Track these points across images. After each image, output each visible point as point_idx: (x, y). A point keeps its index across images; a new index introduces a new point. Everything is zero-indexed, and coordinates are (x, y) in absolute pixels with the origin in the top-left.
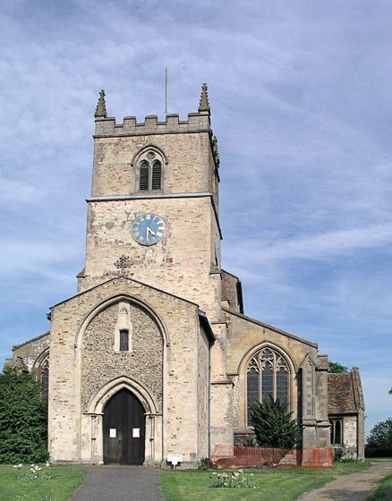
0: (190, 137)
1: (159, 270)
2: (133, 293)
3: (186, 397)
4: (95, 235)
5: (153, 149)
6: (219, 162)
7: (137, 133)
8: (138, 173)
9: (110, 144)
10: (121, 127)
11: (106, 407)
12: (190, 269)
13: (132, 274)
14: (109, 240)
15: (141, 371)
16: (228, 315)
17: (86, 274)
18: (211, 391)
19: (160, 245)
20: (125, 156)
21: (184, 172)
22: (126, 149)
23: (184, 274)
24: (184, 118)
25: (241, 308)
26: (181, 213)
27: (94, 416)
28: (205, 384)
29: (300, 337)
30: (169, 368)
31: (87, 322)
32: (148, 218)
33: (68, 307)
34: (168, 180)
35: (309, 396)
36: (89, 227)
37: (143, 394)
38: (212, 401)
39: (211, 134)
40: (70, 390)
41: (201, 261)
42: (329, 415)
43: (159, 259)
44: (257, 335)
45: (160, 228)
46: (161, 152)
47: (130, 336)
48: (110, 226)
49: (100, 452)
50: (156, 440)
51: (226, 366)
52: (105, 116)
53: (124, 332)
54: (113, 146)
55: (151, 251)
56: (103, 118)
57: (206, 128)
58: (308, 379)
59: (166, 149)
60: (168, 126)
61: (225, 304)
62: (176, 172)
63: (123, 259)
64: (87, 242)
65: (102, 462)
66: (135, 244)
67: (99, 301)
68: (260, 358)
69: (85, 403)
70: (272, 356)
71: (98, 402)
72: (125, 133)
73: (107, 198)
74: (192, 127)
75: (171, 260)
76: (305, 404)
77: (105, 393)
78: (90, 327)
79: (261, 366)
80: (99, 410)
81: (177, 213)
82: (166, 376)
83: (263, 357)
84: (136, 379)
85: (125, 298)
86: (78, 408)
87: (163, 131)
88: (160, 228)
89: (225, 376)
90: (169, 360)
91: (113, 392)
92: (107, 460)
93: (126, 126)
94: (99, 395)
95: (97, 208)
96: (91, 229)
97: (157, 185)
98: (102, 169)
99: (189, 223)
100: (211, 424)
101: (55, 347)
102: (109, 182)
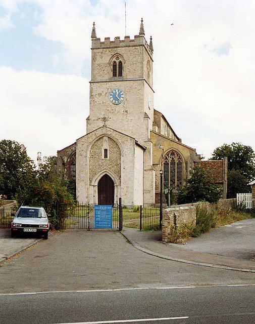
5: (118, 55)
8: (112, 67)
15: (112, 167)
20: (106, 58)
24: (132, 38)
27: (94, 186)
33: (83, 140)
37: (113, 177)
45: (122, 96)
53: (106, 150)
68: (169, 155)
69: (91, 181)
77: (98, 177)
79: (170, 159)
82: (122, 169)
85: (104, 135)
88: (122, 96)
91: (102, 176)
94: (96, 177)
97: (121, 74)
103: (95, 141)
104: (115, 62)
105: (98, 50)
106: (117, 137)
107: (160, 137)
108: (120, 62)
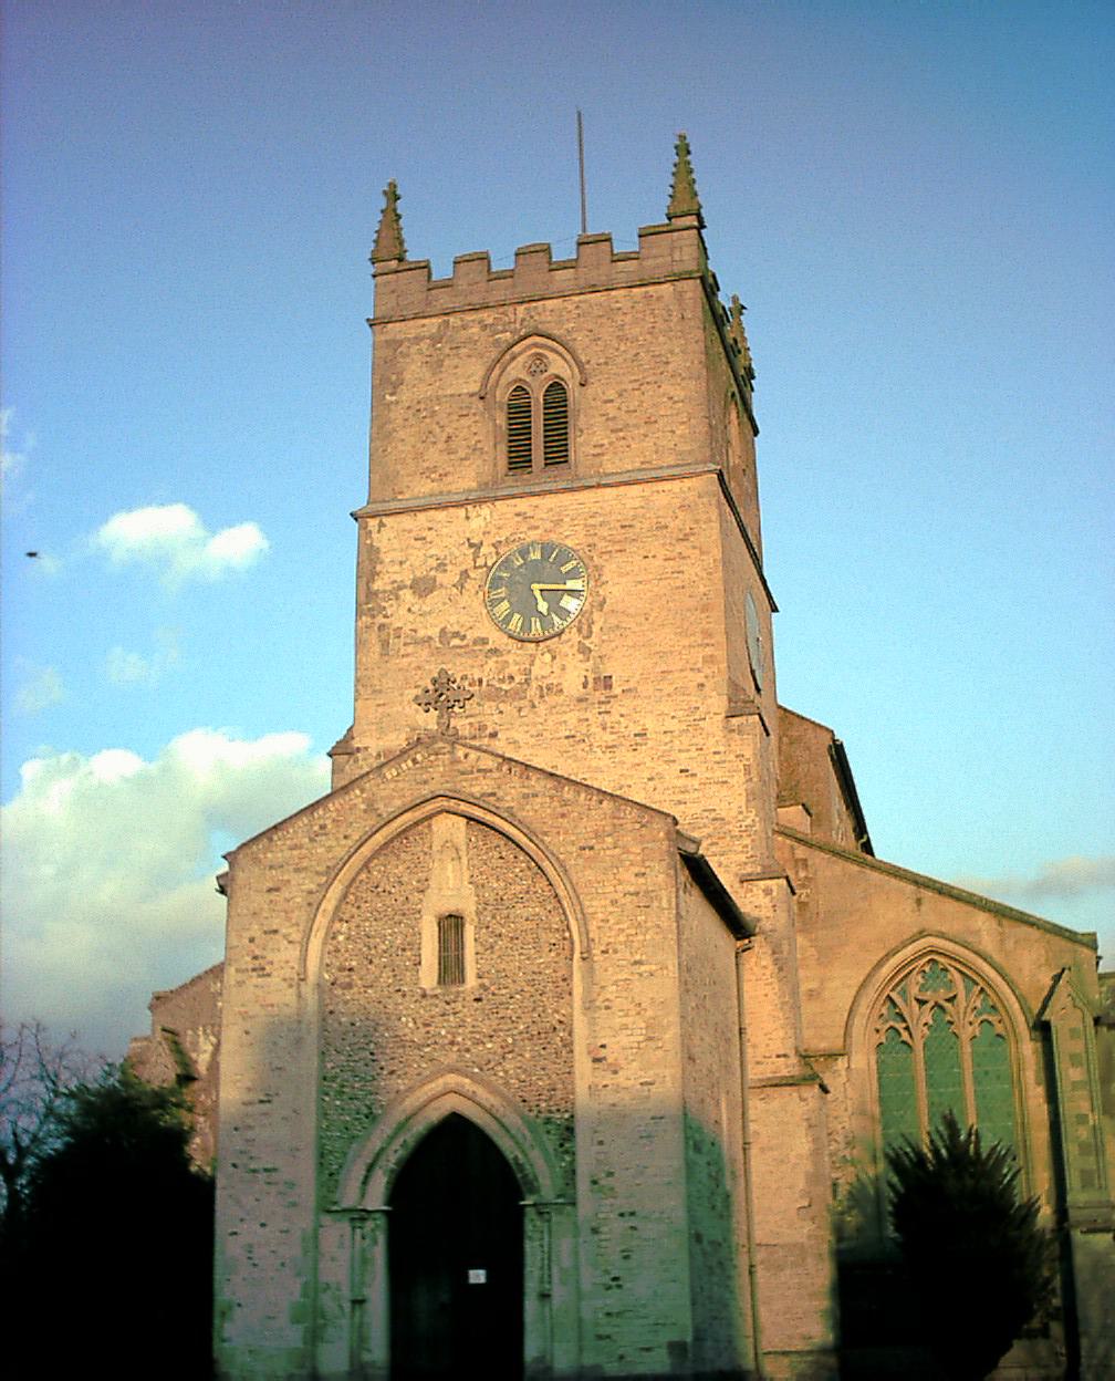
4: (380, 620)
6: (750, 374)
8: (502, 420)
9: (418, 340)
10: (446, 285)
12: (666, 707)
13: (494, 735)
14: (421, 633)
15: (507, 1050)
16: (801, 852)
17: (356, 744)
18: (752, 1114)
19: (573, 636)
21: (634, 405)
22: (463, 351)
23: (650, 723)
25: (860, 828)
26: (630, 534)
27: (360, 1216)
28: (1022, 1192)
30: (593, 1034)
31: (336, 890)
32: (536, 556)
33: (279, 852)
34: (586, 438)
35: (1082, 1119)
36: (363, 598)
39: (710, 287)
41: (700, 678)
44: (893, 913)
47: (469, 932)
48: (423, 587)
50: (556, 1301)
51: (796, 1026)
52: (401, 260)
53: (452, 924)
54: (424, 345)
55: (548, 657)
57: (692, 266)
58: (1074, 1060)
59: (580, 340)
61: (793, 815)
62: (611, 410)
63: (442, 683)
64: (360, 644)
66: (497, 639)
67: (372, 821)
69: (329, 1177)
71: (370, 1168)
72: (458, 302)
74: (655, 263)
75: (607, 682)
76: (1070, 1150)
78: (349, 910)
79: (921, 1018)
80: (376, 1198)
81: (619, 534)
83: (923, 988)
85: (449, 800)
86: (308, 1192)
89: (794, 1060)
90: (589, 1006)
93: (462, 284)
96: (368, 601)
97: (558, 453)
98: (397, 415)
99: (658, 562)
103: (366, 851)
104: (520, 390)
105: (411, 329)
106: (539, 810)
107: (846, 1015)
108: (556, 388)
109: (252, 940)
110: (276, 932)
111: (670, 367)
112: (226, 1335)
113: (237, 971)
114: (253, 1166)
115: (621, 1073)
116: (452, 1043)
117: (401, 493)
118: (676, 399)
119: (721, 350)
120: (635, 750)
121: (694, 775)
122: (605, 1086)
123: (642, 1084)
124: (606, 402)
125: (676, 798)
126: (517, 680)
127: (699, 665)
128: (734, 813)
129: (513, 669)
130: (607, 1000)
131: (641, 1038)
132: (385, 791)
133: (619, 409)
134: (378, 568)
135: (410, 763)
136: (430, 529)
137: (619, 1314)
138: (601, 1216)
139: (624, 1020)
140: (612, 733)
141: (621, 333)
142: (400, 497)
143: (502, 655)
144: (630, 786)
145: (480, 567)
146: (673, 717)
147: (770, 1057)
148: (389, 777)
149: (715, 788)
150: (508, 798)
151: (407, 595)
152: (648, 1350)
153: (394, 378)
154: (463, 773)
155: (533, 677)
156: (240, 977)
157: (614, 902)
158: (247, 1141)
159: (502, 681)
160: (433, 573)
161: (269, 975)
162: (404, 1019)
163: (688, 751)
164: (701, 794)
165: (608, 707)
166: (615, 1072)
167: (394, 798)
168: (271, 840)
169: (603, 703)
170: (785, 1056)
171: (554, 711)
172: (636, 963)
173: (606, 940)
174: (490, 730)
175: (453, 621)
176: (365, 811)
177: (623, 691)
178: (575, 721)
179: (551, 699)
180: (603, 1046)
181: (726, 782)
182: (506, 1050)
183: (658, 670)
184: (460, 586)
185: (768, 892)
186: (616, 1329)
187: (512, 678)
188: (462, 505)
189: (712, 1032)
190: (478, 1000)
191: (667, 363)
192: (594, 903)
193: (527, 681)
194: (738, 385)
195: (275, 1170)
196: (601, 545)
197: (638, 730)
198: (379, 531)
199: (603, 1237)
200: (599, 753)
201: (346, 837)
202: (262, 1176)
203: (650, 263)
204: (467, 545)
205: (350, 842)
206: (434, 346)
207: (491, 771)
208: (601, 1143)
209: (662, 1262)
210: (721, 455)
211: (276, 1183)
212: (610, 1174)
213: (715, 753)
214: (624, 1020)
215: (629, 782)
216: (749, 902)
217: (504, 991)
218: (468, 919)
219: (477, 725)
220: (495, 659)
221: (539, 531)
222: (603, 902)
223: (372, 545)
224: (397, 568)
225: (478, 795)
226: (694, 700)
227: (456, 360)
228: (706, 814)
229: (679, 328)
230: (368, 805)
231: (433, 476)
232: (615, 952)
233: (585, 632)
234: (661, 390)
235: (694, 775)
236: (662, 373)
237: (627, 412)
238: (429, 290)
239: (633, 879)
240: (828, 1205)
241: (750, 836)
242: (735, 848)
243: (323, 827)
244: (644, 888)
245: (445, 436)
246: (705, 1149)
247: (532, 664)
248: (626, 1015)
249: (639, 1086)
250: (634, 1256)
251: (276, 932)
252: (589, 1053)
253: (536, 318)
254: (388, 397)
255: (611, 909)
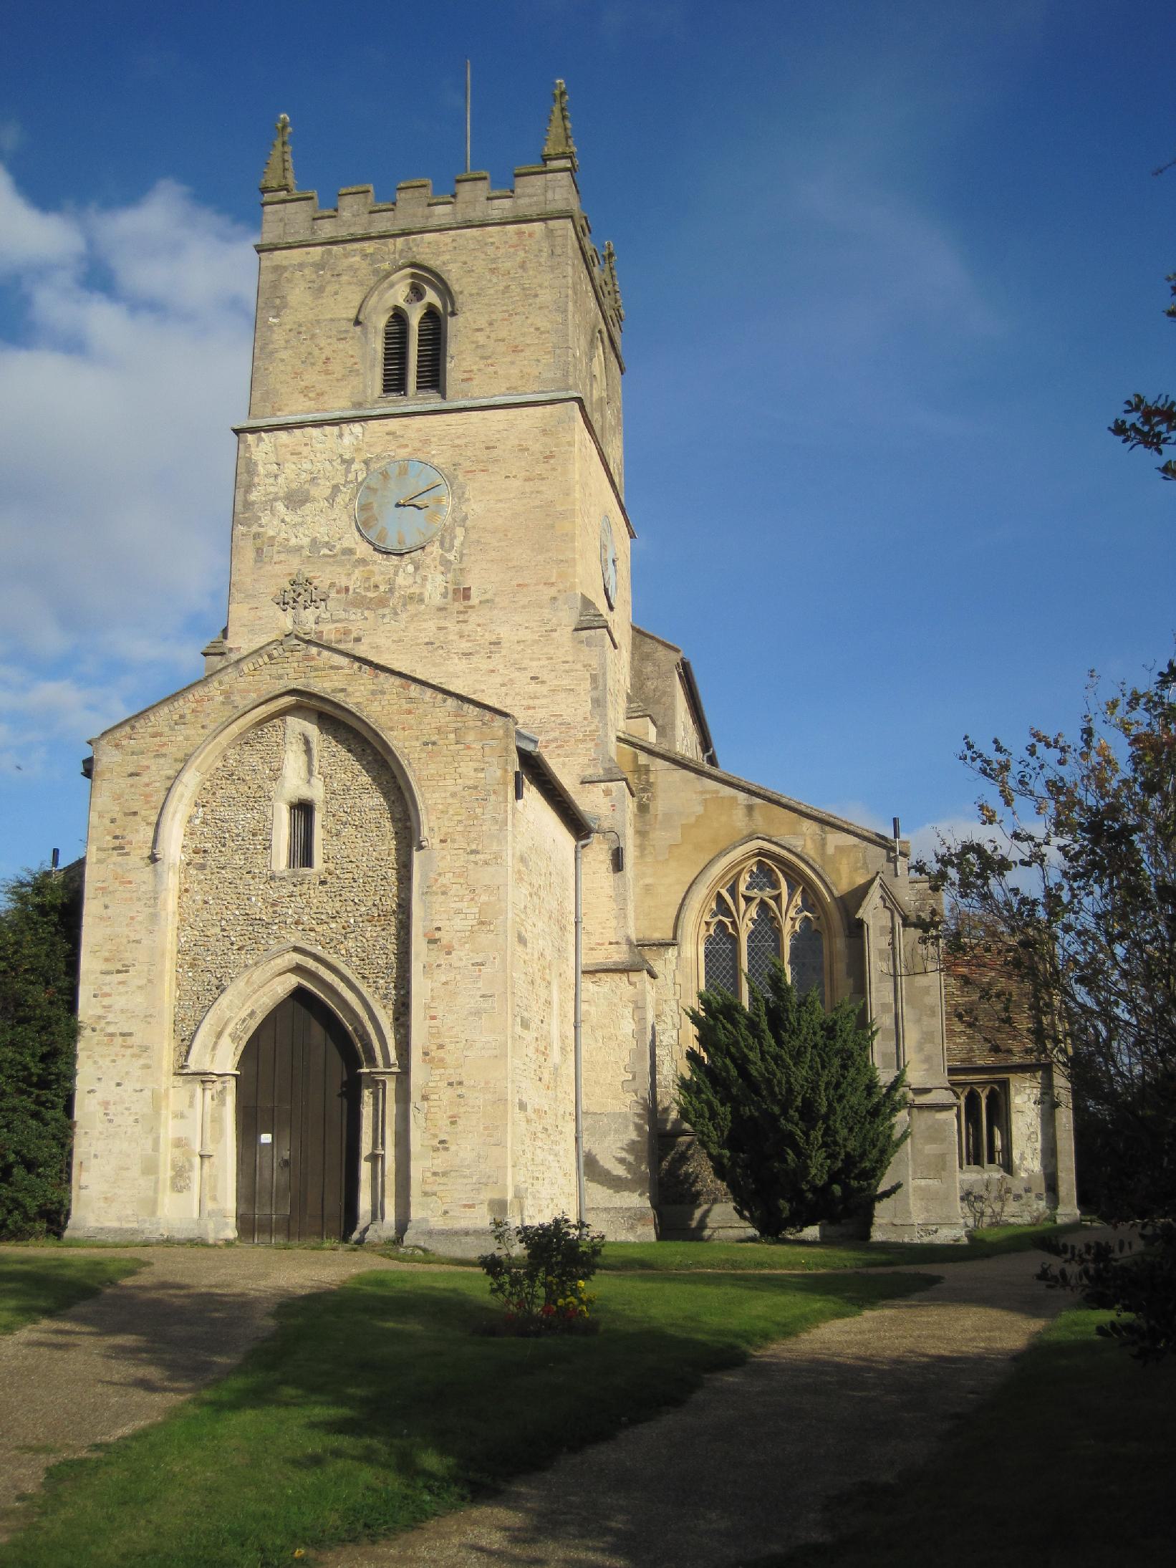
0: (520, 233)
1: (431, 625)
2: (322, 685)
3: (477, 1013)
4: (255, 529)
7: (374, 231)
11: (253, 1053)
13: (358, 640)
14: (293, 541)
16: (643, 758)
18: (583, 996)
19: (435, 549)
22: (344, 278)
23: (504, 632)
29: (396, 666)
36: (239, 508)
38: (584, 1028)
40: (140, 999)
42: (952, 1071)
43: (435, 586)
46: (444, 290)
47: (318, 818)
48: (296, 499)
49: (230, 1203)
53: (303, 809)
54: (307, 271)
55: (410, 568)
56: (283, 194)
60: (460, 206)
62: (481, 338)
65: (231, 1233)
66: (363, 550)
67: (228, 712)
68: (742, 888)
70: (775, 885)
72: (343, 233)
73: (291, 419)
75: (466, 594)
80: (226, 1059)
84: (332, 958)
86: (167, 1056)
87: (445, 221)
89: (625, 947)
92: (247, 1226)
95: (262, 449)
97: (433, 378)
98: (279, 337)
99: (516, 483)
100: (584, 1104)
101: (100, 861)
102: (297, 375)
109: (113, 821)
110: (135, 813)
111: (538, 300)
112: (83, 1183)
113: (99, 849)
114: (111, 1029)
115: (454, 953)
116: (297, 923)
117: (279, 410)
118: (542, 329)
119: (590, 288)
120: (489, 657)
121: (543, 682)
122: (439, 966)
123: (473, 965)
124: (478, 330)
125: (525, 703)
126: (382, 588)
127: (553, 580)
128: (580, 719)
129: (377, 579)
130: (444, 886)
131: (475, 922)
132: (242, 684)
133: (489, 337)
134: (256, 480)
135: (266, 659)
136: (306, 445)
137: (445, 1174)
138: (431, 1084)
139: (459, 905)
140: (468, 641)
141: (494, 266)
142: (279, 413)
143: (368, 565)
144: (483, 691)
145: (351, 482)
146: (527, 628)
147: (603, 944)
148: (246, 671)
149: (564, 695)
150: (358, 694)
151: (280, 506)
152: (471, 1206)
153: (278, 301)
154: (316, 670)
155: (397, 587)
156: (103, 855)
157: (454, 795)
158: (104, 1007)
159: (367, 589)
160: (307, 486)
161: (127, 854)
162: (253, 899)
163: (539, 659)
164: (549, 700)
165: (466, 617)
166: (449, 953)
167: (249, 691)
168: (133, 728)
169: (461, 612)
170: (617, 943)
171: (415, 619)
172: (473, 852)
173: (444, 830)
174: (354, 635)
175: (322, 532)
176: (223, 703)
177: (481, 602)
178: (434, 629)
179: (412, 608)
180: (439, 929)
181: (572, 690)
182: (348, 930)
183: (514, 583)
184: (331, 499)
185: (607, 793)
186: (442, 1187)
187: (376, 587)
188: (337, 424)
189: (546, 919)
190: (323, 883)
191: (536, 296)
192: (434, 796)
193: (391, 591)
194: (606, 324)
195: (130, 1034)
196: (467, 464)
197: (493, 639)
198: (258, 445)
199: (432, 1103)
200: (456, 661)
201: (203, 727)
202: (119, 1040)
203: (521, 201)
204: (339, 460)
205: (207, 732)
206: (317, 272)
207: (342, 668)
208: (433, 1018)
209: (486, 1128)
210: (585, 385)
211: (132, 1047)
212: (441, 1047)
213: (564, 662)
214: (459, 905)
215: (484, 687)
216: (589, 801)
217: (347, 876)
218: (316, 807)
219: (342, 630)
220: (361, 568)
221: (407, 450)
222: (443, 795)
223: (250, 459)
224: (272, 480)
225: (329, 690)
226: (546, 613)
227: (337, 287)
228: (553, 719)
229: (549, 264)
230: (225, 698)
231: (311, 395)
232: (453, 841)
233: (447, 545)
234: (529, 321)
235: (543, 682)
236: (530, 305)
237: (496, 341)
238: (314, 219)
239: (472, 773)
240: (682, 1078)
241: (593, 740)
242: (579, 751)
243: (182, 717)
244: (483, 781)
245: (324, 357)
246: (533, 1026)
247: (396, 574)
248: (462, 901)
249: (470, 967)
250: (460, 1122)
251: (135, 813)
252: (425, 935)
253: (414, 249)
254: (271, 319)
255: (450, 801)
